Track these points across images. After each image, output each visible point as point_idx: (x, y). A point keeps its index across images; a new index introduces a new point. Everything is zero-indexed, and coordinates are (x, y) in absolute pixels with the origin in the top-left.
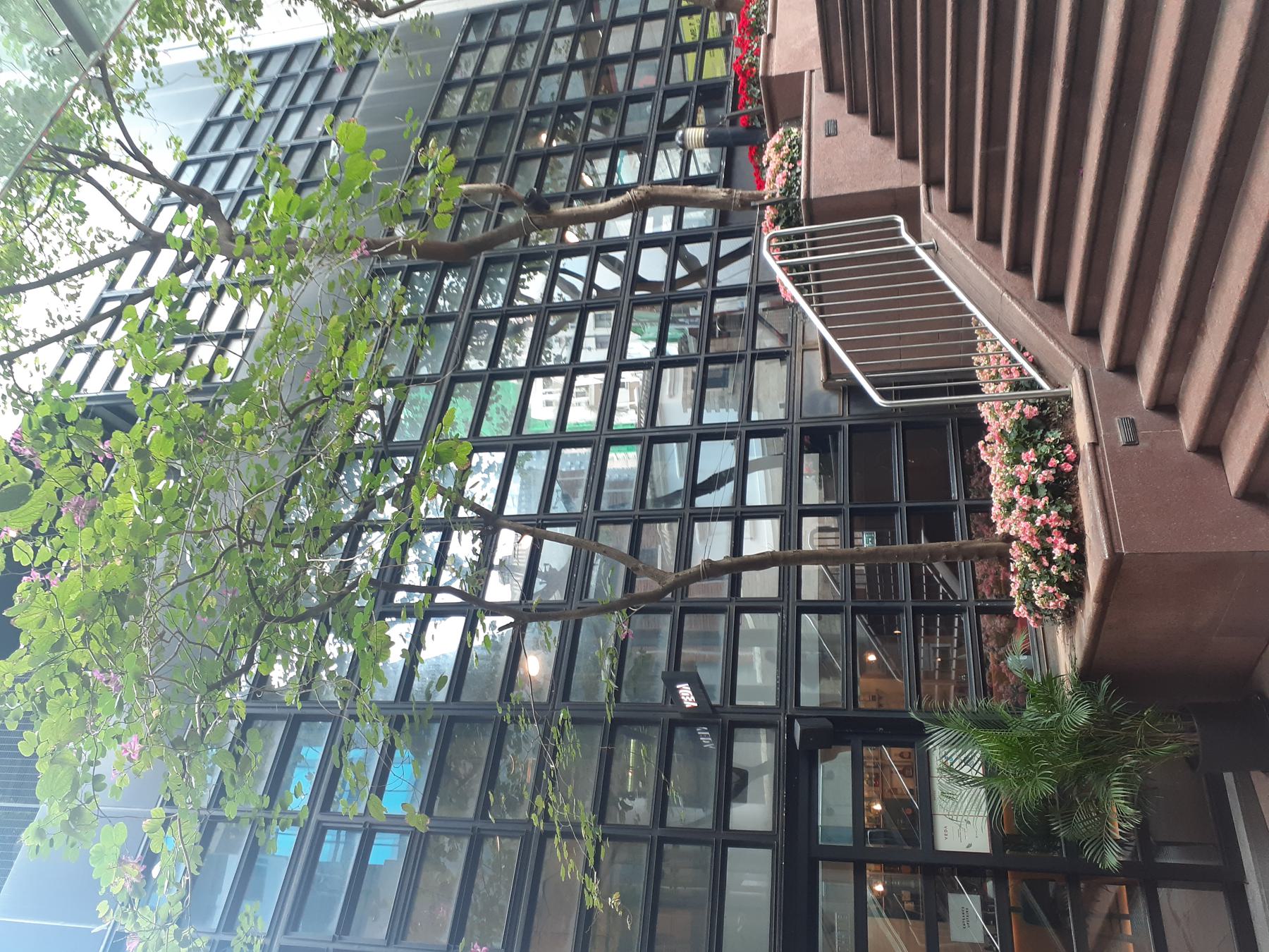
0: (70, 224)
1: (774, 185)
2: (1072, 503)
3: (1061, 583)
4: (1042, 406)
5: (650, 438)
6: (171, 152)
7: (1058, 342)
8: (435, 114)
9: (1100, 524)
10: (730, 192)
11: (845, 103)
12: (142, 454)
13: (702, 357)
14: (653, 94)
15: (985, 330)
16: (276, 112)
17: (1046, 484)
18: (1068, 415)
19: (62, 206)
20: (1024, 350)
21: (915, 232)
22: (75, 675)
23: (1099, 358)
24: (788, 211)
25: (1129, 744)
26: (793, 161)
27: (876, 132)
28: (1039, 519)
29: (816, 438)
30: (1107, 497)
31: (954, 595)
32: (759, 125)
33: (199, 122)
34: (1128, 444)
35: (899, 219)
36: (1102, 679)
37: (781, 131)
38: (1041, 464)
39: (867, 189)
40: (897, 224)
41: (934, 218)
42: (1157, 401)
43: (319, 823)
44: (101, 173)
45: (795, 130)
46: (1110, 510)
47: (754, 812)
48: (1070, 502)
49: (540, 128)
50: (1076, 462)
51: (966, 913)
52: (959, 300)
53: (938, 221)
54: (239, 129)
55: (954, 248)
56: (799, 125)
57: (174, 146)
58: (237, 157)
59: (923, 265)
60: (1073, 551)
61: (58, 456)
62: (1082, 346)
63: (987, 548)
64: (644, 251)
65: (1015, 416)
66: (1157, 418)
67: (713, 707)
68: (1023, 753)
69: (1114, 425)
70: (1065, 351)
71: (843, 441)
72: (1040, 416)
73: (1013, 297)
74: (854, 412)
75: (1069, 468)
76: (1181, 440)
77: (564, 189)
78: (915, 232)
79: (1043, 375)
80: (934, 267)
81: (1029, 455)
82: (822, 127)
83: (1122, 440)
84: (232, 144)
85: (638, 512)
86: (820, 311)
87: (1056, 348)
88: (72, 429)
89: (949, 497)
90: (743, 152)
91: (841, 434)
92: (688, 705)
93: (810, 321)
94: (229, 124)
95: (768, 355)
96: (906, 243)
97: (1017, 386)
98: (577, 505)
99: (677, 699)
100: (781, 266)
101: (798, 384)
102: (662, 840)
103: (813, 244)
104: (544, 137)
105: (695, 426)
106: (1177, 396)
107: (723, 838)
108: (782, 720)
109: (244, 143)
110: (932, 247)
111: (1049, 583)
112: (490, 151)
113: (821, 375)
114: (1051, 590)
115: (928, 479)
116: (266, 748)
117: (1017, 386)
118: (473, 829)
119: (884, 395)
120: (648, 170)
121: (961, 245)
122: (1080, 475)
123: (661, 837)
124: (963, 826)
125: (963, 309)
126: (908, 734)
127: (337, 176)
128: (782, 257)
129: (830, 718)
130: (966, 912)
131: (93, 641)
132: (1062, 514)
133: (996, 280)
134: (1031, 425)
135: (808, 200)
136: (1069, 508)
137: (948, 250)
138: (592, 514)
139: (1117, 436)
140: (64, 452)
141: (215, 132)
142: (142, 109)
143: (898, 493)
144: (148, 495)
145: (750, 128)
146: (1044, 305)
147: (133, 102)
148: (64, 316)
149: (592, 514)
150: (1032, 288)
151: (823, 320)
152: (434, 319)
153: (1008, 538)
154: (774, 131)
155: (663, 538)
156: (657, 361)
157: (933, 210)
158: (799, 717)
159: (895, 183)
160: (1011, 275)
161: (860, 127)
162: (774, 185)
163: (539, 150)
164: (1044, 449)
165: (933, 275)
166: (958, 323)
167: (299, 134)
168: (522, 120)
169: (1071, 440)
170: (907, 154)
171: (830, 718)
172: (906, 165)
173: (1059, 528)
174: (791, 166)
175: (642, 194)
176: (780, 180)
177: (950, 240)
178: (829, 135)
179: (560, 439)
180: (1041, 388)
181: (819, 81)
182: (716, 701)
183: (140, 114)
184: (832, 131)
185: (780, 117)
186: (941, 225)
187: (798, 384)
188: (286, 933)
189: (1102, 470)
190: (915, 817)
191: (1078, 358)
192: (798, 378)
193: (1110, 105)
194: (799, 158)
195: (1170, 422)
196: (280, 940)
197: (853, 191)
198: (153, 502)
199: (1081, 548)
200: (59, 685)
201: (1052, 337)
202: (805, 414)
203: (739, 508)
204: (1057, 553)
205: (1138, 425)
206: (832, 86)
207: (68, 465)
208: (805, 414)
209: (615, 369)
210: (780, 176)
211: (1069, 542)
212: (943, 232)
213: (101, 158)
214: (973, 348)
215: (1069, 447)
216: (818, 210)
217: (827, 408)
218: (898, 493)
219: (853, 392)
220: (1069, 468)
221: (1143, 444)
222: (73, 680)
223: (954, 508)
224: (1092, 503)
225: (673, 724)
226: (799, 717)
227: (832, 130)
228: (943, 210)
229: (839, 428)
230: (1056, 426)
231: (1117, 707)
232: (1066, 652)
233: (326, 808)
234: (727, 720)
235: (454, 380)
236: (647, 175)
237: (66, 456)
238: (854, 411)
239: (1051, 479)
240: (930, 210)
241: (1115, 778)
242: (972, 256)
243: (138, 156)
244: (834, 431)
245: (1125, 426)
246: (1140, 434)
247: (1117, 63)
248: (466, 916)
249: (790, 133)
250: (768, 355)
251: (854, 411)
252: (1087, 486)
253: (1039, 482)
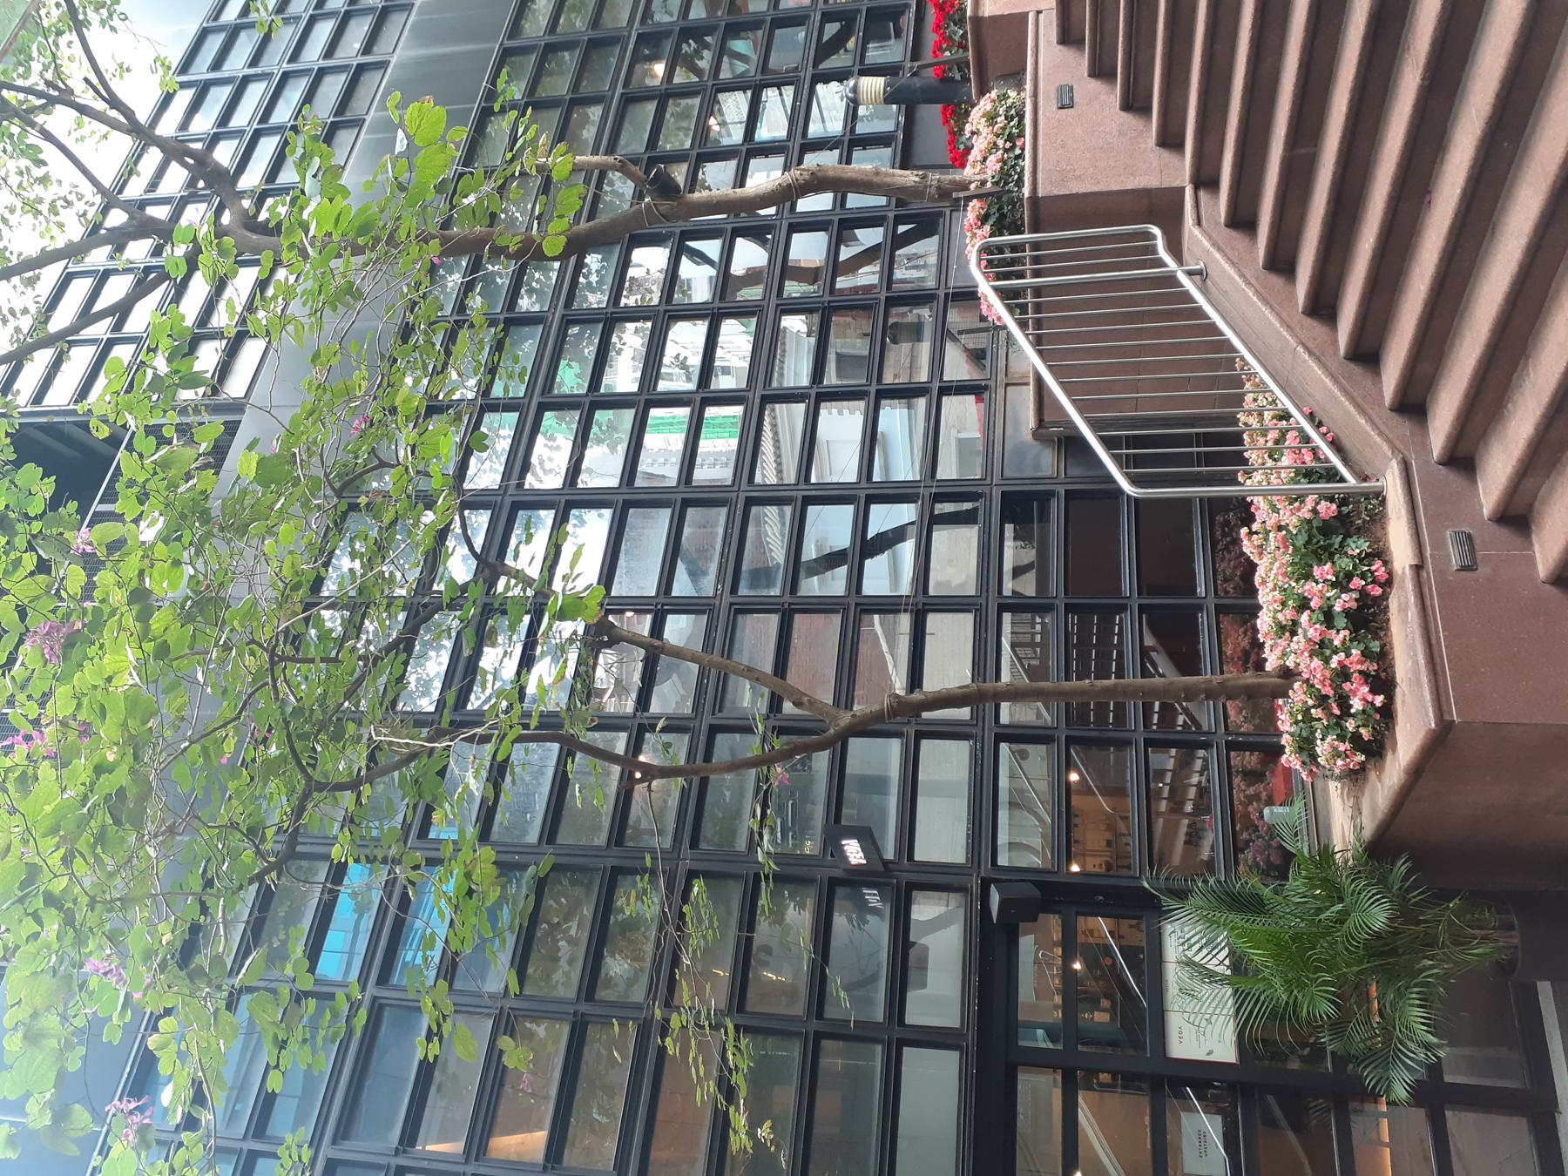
0: (21, 173)
1: (979, 170)
2: (1379, 638)
3: (1356, 739)
4: (1343, 502)
5: (806, 496)
6: (157, 77)
7: (1371, 420)
8: (515, 30)
9: (1425, 679)
10: (924, 177)
11: (1085, 61)
12: (140, 597)
13: (873, 390)
14: (807, 17)
15: (1261, 387)
16: (297, 18)
17: (1347, 613)
18: (1378, 518)
19: (9, 148)
20: (1320, 424)
21: (1175, 249)
22: (54, 911)
23: (1425, 446)
24: (1004, 210)
25: (1430, 942)
26: (1010, 138)
27: (1127, 106)
28: (1335, 659)
29: (1021, 507)
30: (1434, 642)
31: (1198, 726)
32: (958, 77)
33: (192, 29)
34: (1463, 568)
35: (1156, 231)
36: (1398, 857)
37: (994, 94)
38: (1342, 583)
39: (1115, 187)
40: (1154, 237)
41: (1205, 233)
42: (1505, 510)
43: (375, 999)
44: (60, 120)
45: (1012, 94)
46: (1437, 660)
47: (939, 996)
48: (1376, 637)
49: (655, 58)
50: (1388, 584)
51: (1202, 1133)
52: (1222, 334)
53: (1210, 238)
54: (250, 37)
55: (1230, 278)
56: (1020, 87)
57: (160, 70)
58: (246, 81)
59: (1187, 297)
60: (1378, 704)
61: (17, 563)
62: (1402, 426)
63: (1260, 685)
64: (795, 236)
65: (1305, 513)
66: (1503, 533)
67: (886, 863)
68: (1297, 954)
69: (1444, 540)
70: (1381, 433)
71: (1056, 509)
72: (1340, 517)
73: (1311, 353)
74: (1071, 472)
75: (1378, 591)
76: (1534, 565)
77: (687, 145)
78: (1175, 249)
79: (1345, 460)
80: (1215, 317)
81: (1325, 571)
82: (1053, 96)
83: (1455, 563)
84: (237, 63)
85: (787, 598)
86: (1038, 342)
87: (1368, 428)
88: (36, 526)
89: (1192, 590)
90: (931, 114)
91: (1054, 503)
92: (854, 861)
93: (1021, 350)
94: (233, 33)
95: (961, 389)
96: (1165, 265)
97: (1309, 475)
98: (708, 586)
99: (840, 853)
100: (996, 289)
101: (999, 431)
102: (819, 1036)
103: (1036, 260)
104: (659, 69)
105: (864, 484)
106: (1531, 506)
107: (900, 1036)
108: (974, 884)
109: (254, 62)
110: (1200, 273)
111: (1341, 738)
112: (586, 88)
113: (1030, 421)
114: (1342, 747)
115: (1166, 571)
116: (327, 1058)
117: (1309, 475)
118: (575, 1014)
119: (1135, 481)
120: (801, 124)
121: (1242, 276)
122: (1393, 603)
123: (817, 1029)
124: (1202, 1029)
125: (1227, 346)
126: (1140, 907)
127: (404, 178)
128: (999, 277)
129: (1035, 883)
130: (1203, 1136)
131: (79, 860)
132: (1366, 654)
133: (1288, 327)
134: (1327, 528)
135: (1034, 197)
136: (1375, 646)
137: (1215, 271)
138: (727, 599)
139: (1448, 555)
140: (26, 556)
141: (214, 43)
142: (116, 22)
143: (1128, 584)
144: (149, 647)
145: (946, 80)
146: (1352, 365)
147: (104, 12)
148: (18, 308)
149: (727, 599)
150: (1336, 341)
151: (1040, 353)
152: (514, 321)
153: (1288, 674)
154: (983, 90)
155: (771, 526)
156: (813, 392)
157: (1204, 222)
158: (996, 881)
159: (1151, 181)
160: (1309, 321)
161: (1103, 97)
162: (979, 170)
163: (654, 89)
164: (1345, 563)
165: (1199, 313)
166: (1216, 364)
167: (329, 52)
168: (631, 46)
169: (1379, 553)
170: (1170, 140)
171: (1035, 883)
172: (1166, 155)
173: (1361, 672)
174: (1008, 145)
175: (806, 176)
176: (993, 164)
177: (1227, 267)
178: (1062, 107)
179: (685, 498)
180: (1342, 480)
181: (1048, 27)
182: (889, 854)
183: (113, 29)
184: (1066, 101)
185: (990, 72)
186: (1214, 245)
187: (999, 431)
188: (334, 1142)
189: (1428, 603)
190: (1144, 1016)
191: (1397, 443)
192: (999, 423)
193: (1490, 118)
194: (1021, 135)
195: (1518, 540)
196: (327, 1151)
197: (1096, 189)
198: (155, 658)
199: (1390, 699)
200: (30, 926)
201: (1363, 411)
202: (1007, 474)
203: (921, 599)
204: (1357, 705)
205: (1477, 542)
206: (1068, 37)
207: (32, 574)
208: (1007, 474)
209: (757, 400)
210: (992, 158)
211: (1374, 691)
212: (1218, 256)
213: (65, 97)
214: (1238, 400)
215: (1377, 565)
216: (1046, 212)
217: (1037, 467)
218: (1128, 584)
219: (1072, 445)
220: (1378, 591)
221: (1484, 570)
222: (53, 925)
223: (1200, 608)
224: (1411, 647)
225: (834, 883)
226: (996, 881)
227: (1066, 101)
228: (1217, 223)
229: (1051, 494)
230: (1360, 531)
231: (1415, 897)
232: (1346, 821)
233: (383, 980)
234: (902, 881)
235: (543, 408)
236: (800, 130)
237: (29, 561)
238: (1073, 472)
239: (1354, 605)
240: (1199, 223)
241: (1414, 995)
242: (1257, 292)
243: (114, 102)
244: (1045, 497)
245: (1460, 544)
246: (1480, 554)
247: (1509, 62)
248: (568, 1121)
249: (1006, 97)
250: (961, 389)
251: (1073, 472)
252: (1405, 622)
253: (1338, 608)
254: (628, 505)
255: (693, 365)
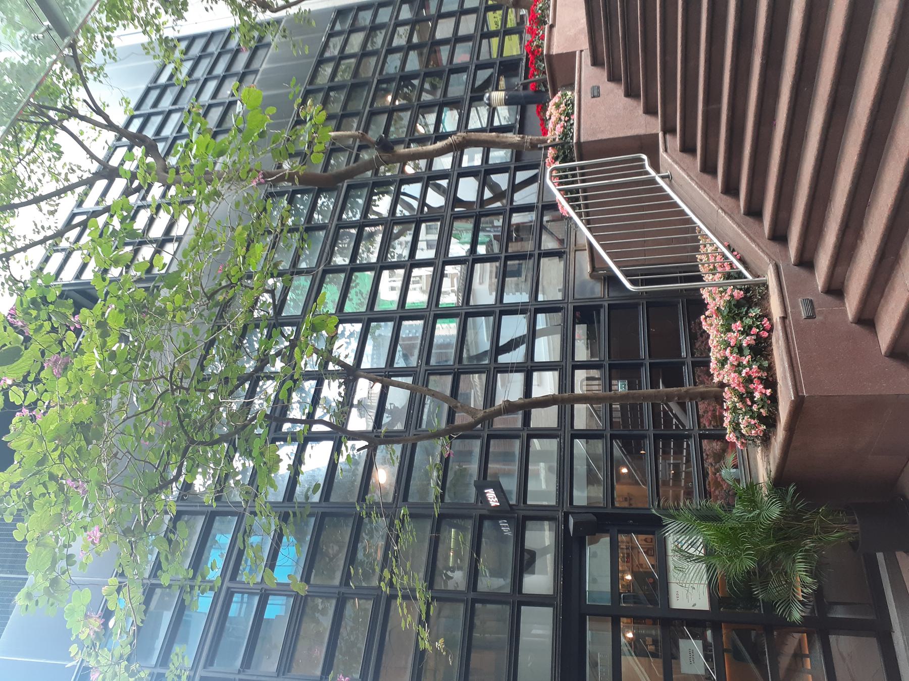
0: (50, 160)
1: (554, 133)
2: (768, 360)
3: (760, 417)
4: (747, 291)
5: (465, 313)
6: (122, 109)
7: (758, 245)
8: (311, 81)
9: (788, 375)
10: (523, 138)
11: (605, 74)
12: (102, 325)
13: (503, 256)
14: (468, 68)
15: (705, 236)
16: (198, 80)
17: (750, 346)
18: (765, 297)
19: (45, 148)
20: (734, 250)
21: (656, 166)
22: (54, 483)
23: (787, 256)
24: (564, 151)
25: (809, 532)
26: (568, 115)
27: (628, 94)
28: (744, 371)
29: (584, 313)
30: (793, 356)
31: (684, 426)
32: (543, 89)
33: (142, 87)
34: (808, 317)
35: (644, 157)
36: (789, 486)
37: (559, 94)
38: (746, 332)
39: (621, 135)
40: (643, 160)
41: (669, 156)
42: (829, 287)
43: (228, 588)
44: (72, 124)
45: (569, 93)
46: (795, 365)
47: (540, 581)
48: (766, 359)
49: (387, 91)
50: (771, 331)
51: (692, 653)
52: (687, 215)
53: (672, 158)
54: (171, 93)
55: (683, 178)
56: (573, 90)
57: (124, 104)
58: (170, 112)
59: (661, 189)
60: (768, 394)
61: (41, 326)
62: (775, 247)
63: (707, 392)
64: (461, 180)
65: (727, 298)
66: (829, 299)
67: (511, 506)
68: (733, 538)
69: (798, 304)
70: (763, 251)
71: (604, 315)
72: (745, 298)
73: (725, 213)
74: (611, 294)
75: (766, 335)
76: (846, 315)
77: (404, 135)
78: (656, 166)
79: (747, 268)
80: (669, 191)
81: (737, 326)
82: (589, 91)
83: (803, 315)
84: (166, 103)
85: (457, 366)
86: (588, 223)
87: (757, 249)
88: (51, 307)
89: (680, 356)
90: (532, 109)
91: (602, 311)
92: (493, 504)
93: (581, 230)
94: (164, 89)
95: (550, 254)
96: (649, 174)
97: (728, 276)
98: (414, 362)
99: (485, 500)
100: (560, 190)
101: (572, 275)
102: (474, 601)
103: (582, 175)
104: (389, 98)
105: (498, 305)
106: (843, 283)
107: (518, 600)
108: (560, 515)
109: (175, 102)
110: (668, 177)
111: (751, 417)
112: (351, 108)
113: (588, 268)
114: (753, 422)
115: (665, 343)
116: (190, 535)
117: (728, 276)
118: (339, 593)
119: (633, 283)
120: (464, 122)
121: (689, 176)
122: (774, 340)
123: (473, 599)
124: (690, 591)
125: (690, 221)
126: (650, 525)
127: (241, 126)
128: (560, 184)
129: (594, 514)
130: (692, 652)
131: (67, 459)
132: (761, 368)
133: (713, 200)
134: (739, 304)
135: (579, 143)
136: (766, 364)
137: (679, 179)
138: (424, 367)
139: (800, 312)
140: (46, 323)
141: (154, 94)
142: (102, 78)
143: (643, 352)
144: (106, 354)
145: (537, 92)
146: (748, 218)
147: (95, 73)
148: (46, 226)
149: (424, 367)
150: (739, 206)
151: (589, 229)
152: (311, 228)
153: (722, 385)
154: (554, 94)
155: (475, 385)
156: (471, 259)
157: (669, 150)
158: (572, 513)
159: (641, 131)
160: (724, 197)
161: (616, 91)
162: (554, 133)
163: (386, 107)
164: (748, 321)
165: (668, 197)
166: (686, 231)
167: (214, 96)
168: (374, 86)
169: (767, 315)
170: (650, 110)
171: (594, 514)
172: (649, 118)
173: (759, 378)
174: (567, 118)
175: (460, 139)
176: (559, 129)
177: (681, 171)
178: (594, 97)
179: (401, 314)
180: (745, 278)
181: (586, 58)
182: (513, 502)
183: (100, 81)
184: (596, 94)
185: (559, 84)
186: (674, 161)
187: (572, 275)
188: (205, 667)
189: (790, 336)
190: (656, 584)
191: (772, 256)
192: (572, 270)
193: (795, 75)
194: (573, 113)
195: (838, 302)
196: (201, 672)
197: (611, 137)
198: (110, 359)
199: (775, 392)
200: (42, 490)
201: (754, 241)
202: (576, 296)
203: (529, 364)
204: (757, 395)
205: (815, 304)
206: (596, 62)
207: (48, 332)
208: (576, 296)
209: (441, 264)
210: (559, 126)
211: (766, 388)
212: (676, 166)
213: (72, 113)
214: (697, 249)
215: (765, 320)
216: (586, 150)
217: (593, 292)
218: (643, 352)
219: (611, 280)
220: (766, 335)
221: (819, 318)
222: (53, 487)
223: (683, 364)
224: (782, 360)
225: (482, 518)
226: (572, 513)
227: (596, 93)
228: (675, 150)
229: (601, 306)
230: (756, 305)
231: (800, 505)
232: (764, 466)
233: (233, 578)
234: (521, 515)
235: (325, 272)
236: (464, 125)
237: (47, 326)
238: (612, 294)
239: (753, 342)
240: (666, 150)
241: (799, 556)
242: (697, 183)
243: (99, 112)
244: (598, 308)
245: (805, 305)
246: (817, 310)
247: (800, 45)
248: (334, 655)
249: (566, 95)
250: (550, 254)
251: (612, 294)
252: (778, 348)
253: (744, 345)
254: (474, 601)
255: (419, 280)
